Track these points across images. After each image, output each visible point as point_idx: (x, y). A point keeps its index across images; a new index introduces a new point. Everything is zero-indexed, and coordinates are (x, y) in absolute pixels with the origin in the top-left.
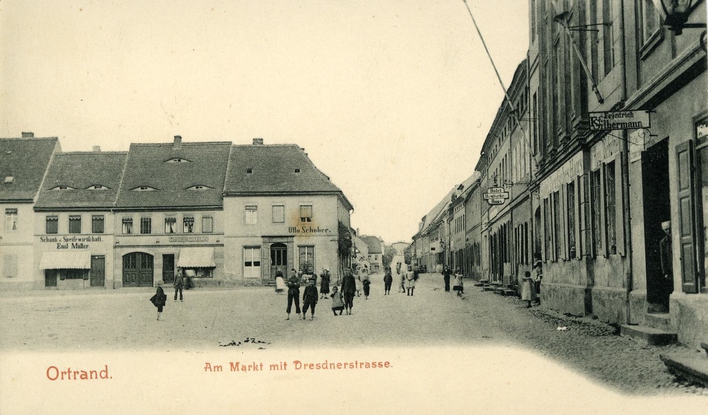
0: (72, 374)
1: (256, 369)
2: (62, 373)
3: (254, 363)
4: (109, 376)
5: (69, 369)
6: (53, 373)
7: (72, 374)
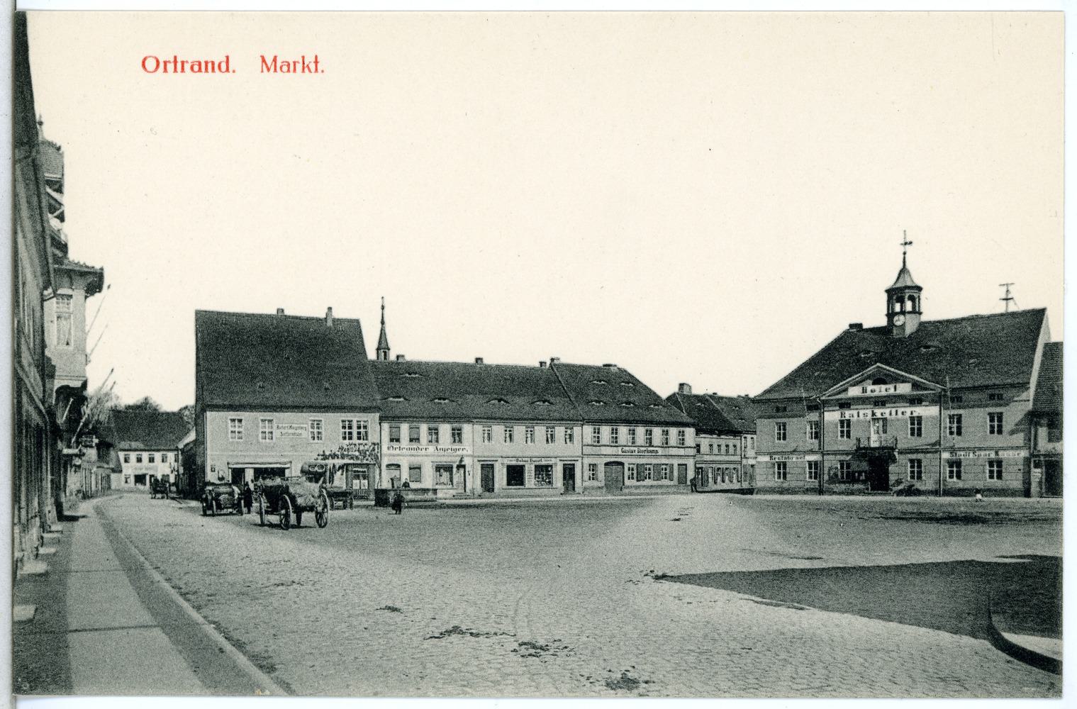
0: (179, 66)
1: (306, 70)
2: (165, 63)
3: (303, 57)
4: (231, 69)
5: (175, 57)
6: (151, 64)
7: (179, 66)
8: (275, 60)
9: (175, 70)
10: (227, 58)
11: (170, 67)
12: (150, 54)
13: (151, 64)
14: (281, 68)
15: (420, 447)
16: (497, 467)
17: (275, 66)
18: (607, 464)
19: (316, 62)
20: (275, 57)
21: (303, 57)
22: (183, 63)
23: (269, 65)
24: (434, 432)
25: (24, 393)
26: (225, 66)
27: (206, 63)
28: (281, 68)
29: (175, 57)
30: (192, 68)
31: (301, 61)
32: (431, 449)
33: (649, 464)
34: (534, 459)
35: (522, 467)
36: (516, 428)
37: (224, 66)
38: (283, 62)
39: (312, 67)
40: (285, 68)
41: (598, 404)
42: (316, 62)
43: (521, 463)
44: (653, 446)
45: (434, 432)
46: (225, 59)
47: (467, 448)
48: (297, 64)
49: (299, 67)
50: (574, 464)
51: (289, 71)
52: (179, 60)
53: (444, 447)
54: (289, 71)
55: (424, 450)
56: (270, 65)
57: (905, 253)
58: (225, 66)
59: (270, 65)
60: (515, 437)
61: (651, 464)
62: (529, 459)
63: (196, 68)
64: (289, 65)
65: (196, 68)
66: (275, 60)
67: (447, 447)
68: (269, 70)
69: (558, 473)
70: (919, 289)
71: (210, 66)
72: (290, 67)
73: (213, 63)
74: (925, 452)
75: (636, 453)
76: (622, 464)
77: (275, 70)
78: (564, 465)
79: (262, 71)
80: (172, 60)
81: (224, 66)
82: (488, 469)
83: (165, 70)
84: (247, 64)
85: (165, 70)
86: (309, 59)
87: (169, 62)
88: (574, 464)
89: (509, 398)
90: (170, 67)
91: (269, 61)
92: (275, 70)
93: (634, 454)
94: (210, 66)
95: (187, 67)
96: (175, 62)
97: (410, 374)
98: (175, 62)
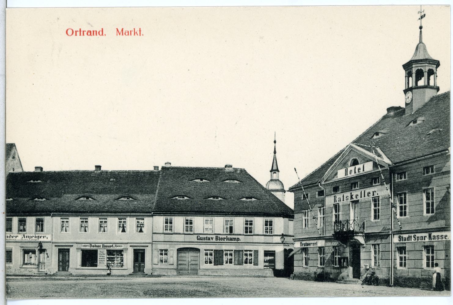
0: (82, 33)
1: (136, 34)
2: (76, 31)
3: (134, 29)
4: (104, 34)
5: (80, 29)
6: (70, 32)
7: (82, 33)
8: (122, 30)
9: (80, 35)
10: (102, 29)
11: (78, 33)
12: (69, 28)
13: (70, 32)
14: (125, 33)
15: (12, 235)
16: (72, 251)
17: (123, 33)
18: (180, 250)
19: (140, 31)
20: (117, 29)
21: (134, 29)
22: (83, 31)
23: (120, 32)
24: (22, 222)
25: (223, 199)
26: (101, 33)
27: (93, 31)
28: (125, 33)
29: (80, 29)
30: (87, 34)
31: (133, 30)
32: (20, 237)
33: (230, 250)
34: (105, 245)
35: (96, 251)
36: (128, 219)
37: (101, 33)
38: (89, 31)
39: (138, 33)
40: (127, 34)
41: (181, 199)
42: (140, 31)
43: (95, 248)
44: (234, 235)
45: (22, 222)
46: (101, 30)
47: (47, 236)
48: (84, 32)
49: (133, 33)
50: (144, 250)
51: (128, 35)
52: (82, 30)
53: (29, 236)
54: (128, 35)
55: (14, 238)
56: (120, 32)
57: (421, 28)
58: (101, 33)
59: (120, 32)
60: (128, 229)
61: (212, 250)
62: (101, 245)
63: (89, 34)
64: (128, 33)
65: (89, 34)
66: (122, 30)
67: (31, 235)
68: (120, 34)
69: (129, 258)
70: (437, 64)
71: (95, 32)
72: (129, 33)
73: (96, 32)
74: (228, 235)
75: (214, 240)
76: (198, 250)
77: (123, 35)
78: (59, 249)
79: (117, 35)
80: (79, 30)
81: (101, 33)
82: (64, 252)
83: (76, 35)
84: (110, 32)
85: (76, 35)
86: (137, 30)
87: (78, 31)
88: (144, 250)
89: (95, 196)
90: (78, 33)
91: (120, 31)
92: (123, 35)
93: (211, 241)
94: (95, 32)
95: (85, 33)
96: (80, 31)
97: (202, 180)
98: (80, 31)
